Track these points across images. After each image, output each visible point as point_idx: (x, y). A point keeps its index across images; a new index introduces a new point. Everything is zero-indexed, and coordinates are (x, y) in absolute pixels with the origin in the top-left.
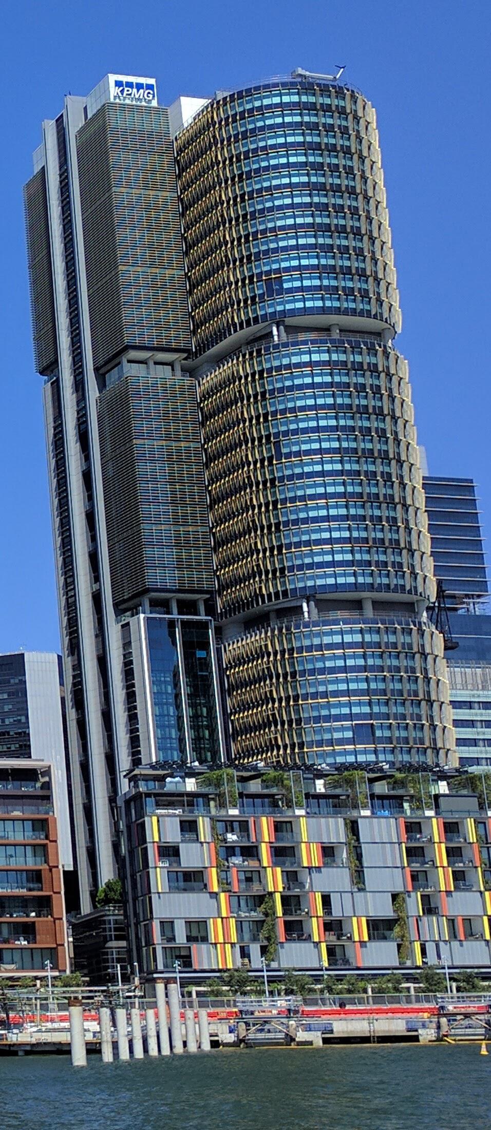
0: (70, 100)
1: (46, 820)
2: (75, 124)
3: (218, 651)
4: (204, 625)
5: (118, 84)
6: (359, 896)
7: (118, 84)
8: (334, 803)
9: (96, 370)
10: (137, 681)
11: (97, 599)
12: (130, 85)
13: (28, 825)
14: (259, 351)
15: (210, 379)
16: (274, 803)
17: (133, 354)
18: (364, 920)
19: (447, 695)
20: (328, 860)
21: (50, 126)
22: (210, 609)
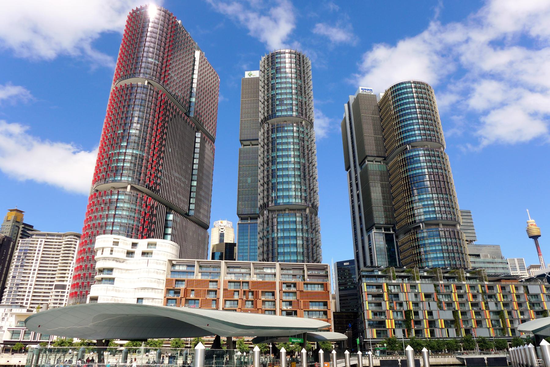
0: (350, 96)
1: (327, 302)
2: (352, 102)
3: (397, 242)
4: (392, 234)
5: (362, 89)
6: (440, 311)
7: (362, 89)
8: (432, 278)
9: (360, 165)
10: (373, 252)
11: (361, 229)
12: (365, 89)
13: (322, 303)
14: (416, 232)
15: (390, 164)
16: (409, 278)
17: (369, 158)
18: (443, 320)
19: (465, 239)
20: (493, 297)
21: (346, 105)
22: (394, 230)
